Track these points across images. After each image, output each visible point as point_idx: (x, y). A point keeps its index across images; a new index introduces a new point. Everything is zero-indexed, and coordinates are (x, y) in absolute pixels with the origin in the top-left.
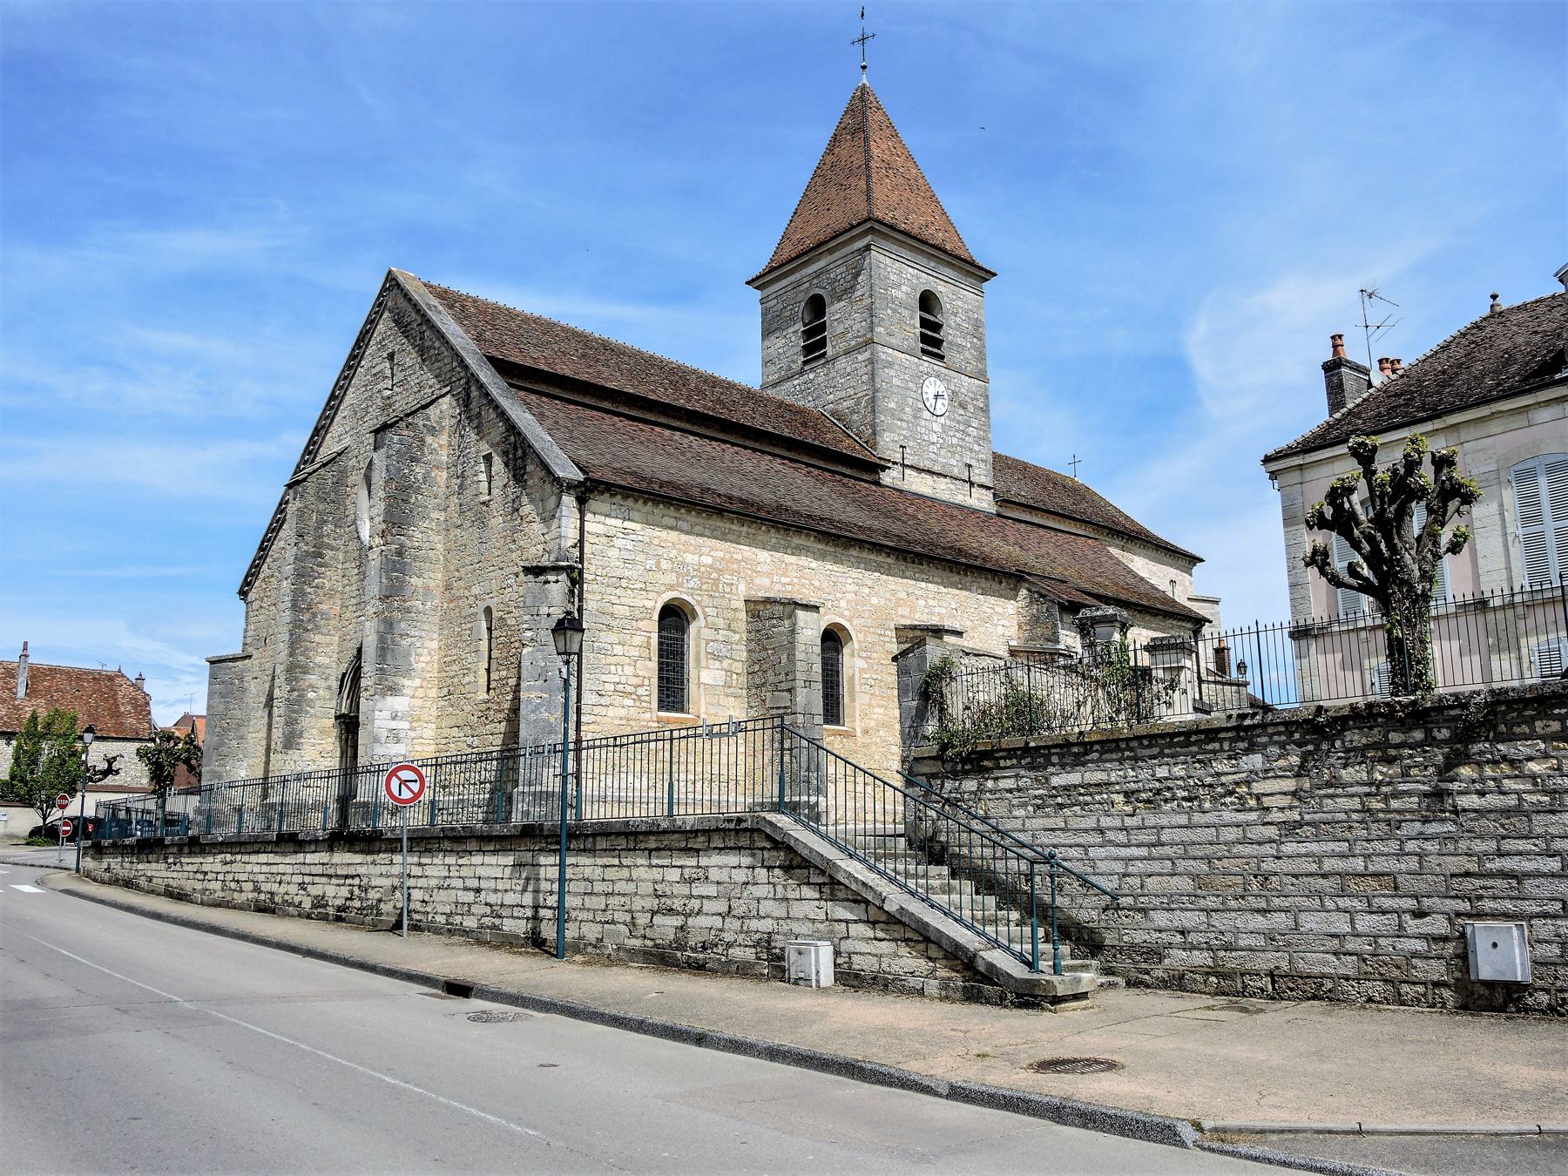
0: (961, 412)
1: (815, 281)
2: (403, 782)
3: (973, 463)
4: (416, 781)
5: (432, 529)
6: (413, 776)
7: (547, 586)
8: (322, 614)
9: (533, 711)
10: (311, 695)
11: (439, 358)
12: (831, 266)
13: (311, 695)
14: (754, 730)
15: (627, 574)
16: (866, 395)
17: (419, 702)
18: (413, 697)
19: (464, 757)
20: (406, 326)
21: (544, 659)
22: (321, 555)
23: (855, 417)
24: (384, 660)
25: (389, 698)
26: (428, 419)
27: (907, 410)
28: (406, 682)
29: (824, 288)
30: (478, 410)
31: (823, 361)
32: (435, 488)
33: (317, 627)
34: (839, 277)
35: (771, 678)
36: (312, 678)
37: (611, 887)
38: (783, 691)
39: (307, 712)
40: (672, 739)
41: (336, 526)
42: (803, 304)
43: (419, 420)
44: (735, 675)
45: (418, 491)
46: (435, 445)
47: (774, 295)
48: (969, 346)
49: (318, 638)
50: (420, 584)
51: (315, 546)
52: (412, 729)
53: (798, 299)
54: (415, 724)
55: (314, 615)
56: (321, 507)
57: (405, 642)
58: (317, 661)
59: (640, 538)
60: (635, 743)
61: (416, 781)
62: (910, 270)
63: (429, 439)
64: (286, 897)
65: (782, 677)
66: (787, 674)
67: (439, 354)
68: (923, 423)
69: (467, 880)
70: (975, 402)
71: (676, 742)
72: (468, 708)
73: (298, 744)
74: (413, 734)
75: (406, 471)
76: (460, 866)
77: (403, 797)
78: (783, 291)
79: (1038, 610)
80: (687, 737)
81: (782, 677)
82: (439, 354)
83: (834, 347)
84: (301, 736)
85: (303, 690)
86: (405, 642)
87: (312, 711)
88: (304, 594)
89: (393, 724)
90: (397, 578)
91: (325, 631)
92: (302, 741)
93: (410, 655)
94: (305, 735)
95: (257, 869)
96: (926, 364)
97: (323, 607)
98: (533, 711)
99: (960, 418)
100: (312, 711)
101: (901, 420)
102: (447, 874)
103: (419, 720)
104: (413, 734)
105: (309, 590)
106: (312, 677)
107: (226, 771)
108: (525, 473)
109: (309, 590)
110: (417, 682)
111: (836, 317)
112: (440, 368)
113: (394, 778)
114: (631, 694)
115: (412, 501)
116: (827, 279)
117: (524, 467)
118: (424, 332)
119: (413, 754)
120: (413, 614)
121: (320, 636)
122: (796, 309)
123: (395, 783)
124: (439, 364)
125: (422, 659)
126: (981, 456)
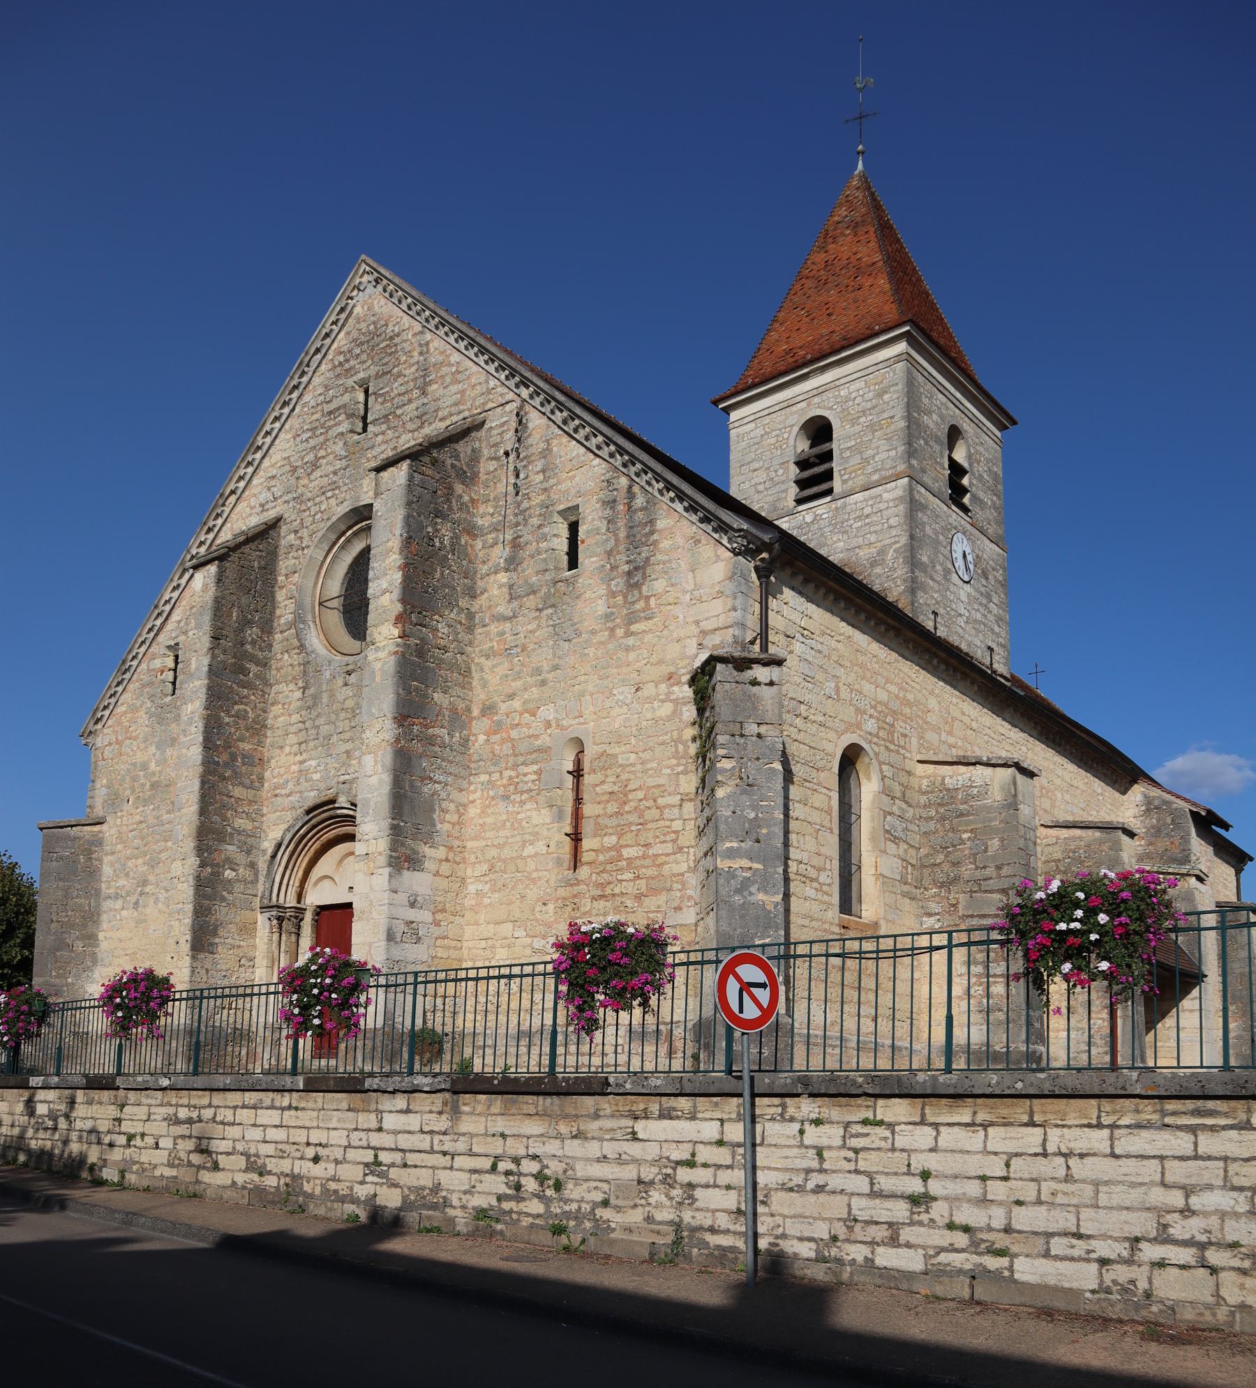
0: (984, 582)
1: (816, 400)
2: (746, 987)
3: (994, 646)
4: (763, 986)
5: (460, 623)
6: (760, 977)
7: (755, 689)
8: (244, 757)
9: (738, 891)
10: (228, 874)
11: (459, 377)
12: (842, 381)
13: (228, 874)
14: (811, 956)
15: (807, 697)
16: (896, 542)
17: (444, 884)
18: (437, 874)
19: (220, 991)
20: (391, 338)
21: (754, 807)
22: (246, 672)
23: (878, 570)
24: (401, 816)
25: (406, 873)
26: (457, 458)
27: (938, 567)
28: (427, 850)
29: (831, 408)
30: (542, 446)
31: (828, 499)
32: (464, 562)
33: (236, 774)
34: (854, 395)
35: (967, 870)
36: (231, 849)
37: (436, 1142)
38: (991, 892)
39: (223, 899)
40: (416, 984)
41: (262, 631)
42: (796, 429)
43: (444, 455)
44: (910, 867)
45: (444, 562)
46: (466, 498)
47: (752, 418)
48: (989, 503)
49: (238, 792)
50: (446, 703)
51: (235, 657)
52: (437, 924)
53: (789, 422)
54: (439, 916)
55: (233, 758)
56: (244, 600)
57: (427, 789)
58: (236, 825)
59: (819, 647)
60: (268, 994)
61: (763, 986)
62: (940, 396)
63: (459, 488)
64: (333, 1186)
65: (990, 871)
66: (999, 868)
67: (458, 372)
68: (952, 588)
69: (867, 1190)
70: (995, 573)
71: (421, 988)
72: (533, 893)
73: (212, 944)
74: (436, 931)
75: (430, 529)
76: (856, 1151)
77: (745, 1016)
78: (766, 412)
79: (1158, 821)
80: (488, 978)
81: (990, 871)
82: (458, 372)
83: (844, 482)
84: (215, 934)
85: (218, 865)
86: (427, 789)
87: (230, 897)
88: (220, 726)
89: (412, 914)
90: (417, 689)
91: (247, 782)
92: (217, 940)
93: (432, 810)
94: (221, 932)
95: (256, 1134)
96: (954, 515)
97: (245, 746)
98: (738, 891)
99: (983, 589)
100: (230, 897)
101: (933, 579)
102: (815, 1164)
103: (443, 911)
104: (436, 931)
105: (227, 720)
106: (229, 847)
107: (67, 985)
108: (652, 533)
109: (227, 720)
110: (441, 852)
111: (849, 445)
112: (463, 392)
113: (731, 979)
114: (812, 880)
115: (437, 575)
116: (836, 397)
117: (652, 522)
118: (427, 344)
119: (436, 961)
120: (437, 749)
121: (240, 788)
122: (786, 436)
123: (732, 987)
124: (460, 386)
125: (448, 817)
126: (1000, 640)
